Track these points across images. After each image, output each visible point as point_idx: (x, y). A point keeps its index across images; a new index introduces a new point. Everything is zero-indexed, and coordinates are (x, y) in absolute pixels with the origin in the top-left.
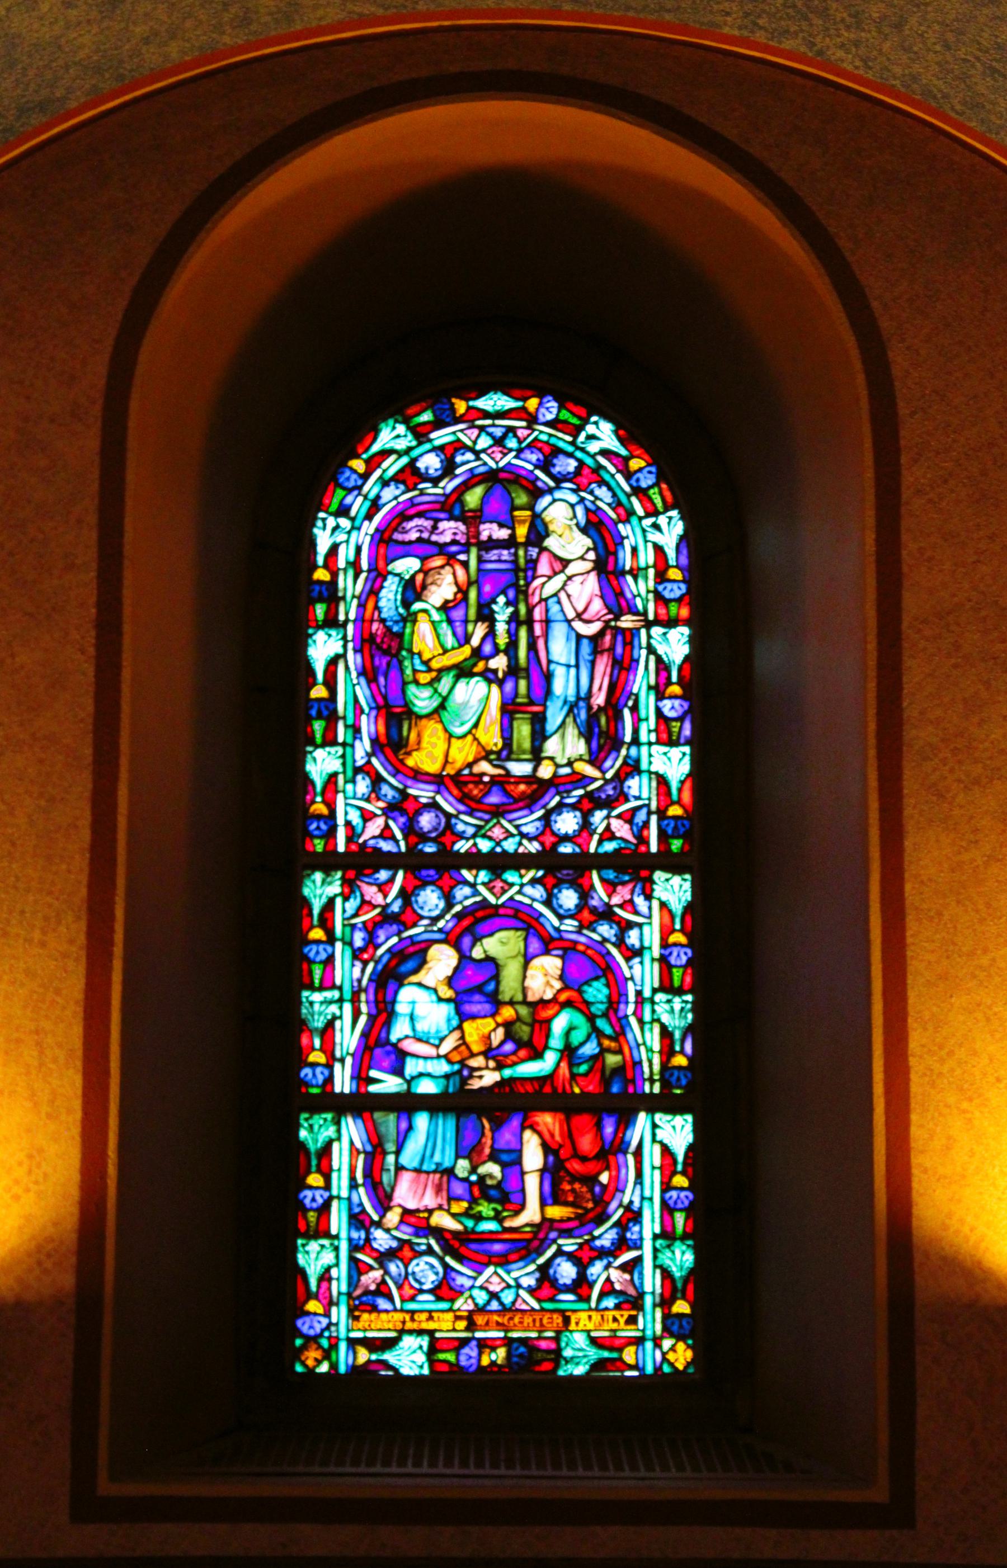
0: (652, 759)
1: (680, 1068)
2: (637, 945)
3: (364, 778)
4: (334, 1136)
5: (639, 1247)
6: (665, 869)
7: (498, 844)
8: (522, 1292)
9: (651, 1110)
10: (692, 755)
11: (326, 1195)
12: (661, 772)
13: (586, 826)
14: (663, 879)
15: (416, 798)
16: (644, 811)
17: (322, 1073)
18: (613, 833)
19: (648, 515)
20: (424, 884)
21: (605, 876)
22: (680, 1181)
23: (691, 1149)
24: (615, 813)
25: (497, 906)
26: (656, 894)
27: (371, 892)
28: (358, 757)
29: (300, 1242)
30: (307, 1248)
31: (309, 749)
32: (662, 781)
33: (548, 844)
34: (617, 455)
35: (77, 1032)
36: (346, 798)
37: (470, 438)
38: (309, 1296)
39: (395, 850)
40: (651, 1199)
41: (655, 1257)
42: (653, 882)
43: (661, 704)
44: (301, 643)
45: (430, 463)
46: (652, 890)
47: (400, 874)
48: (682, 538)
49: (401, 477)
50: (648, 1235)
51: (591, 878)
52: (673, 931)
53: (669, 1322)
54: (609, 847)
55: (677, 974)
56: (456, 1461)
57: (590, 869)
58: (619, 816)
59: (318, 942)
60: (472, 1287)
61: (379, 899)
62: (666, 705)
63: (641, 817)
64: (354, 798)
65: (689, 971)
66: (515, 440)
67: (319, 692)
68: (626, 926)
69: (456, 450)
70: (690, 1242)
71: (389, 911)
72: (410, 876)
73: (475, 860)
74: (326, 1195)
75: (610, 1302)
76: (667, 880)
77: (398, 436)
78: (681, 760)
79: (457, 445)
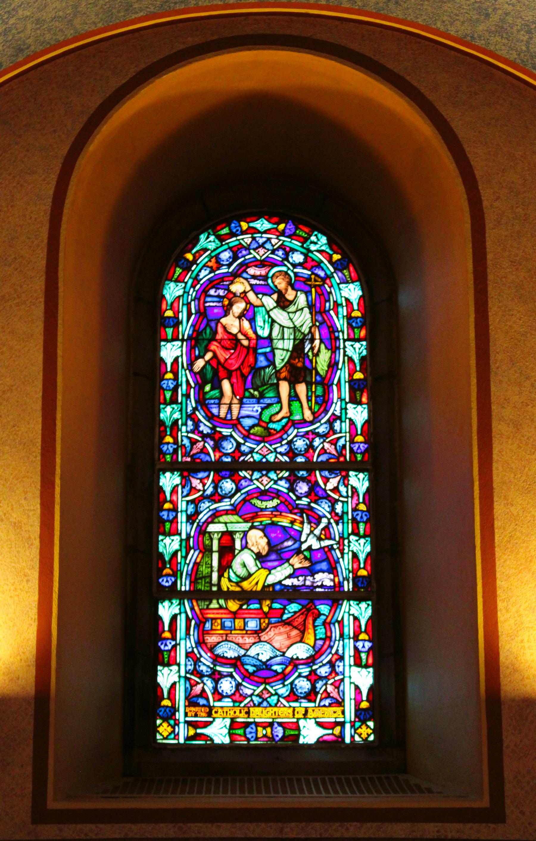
0: (351, 607)
3: (193, 508)
7: (264, 457)
8: (281, 699)
9: (349, 600)
10: (372, 605)
11: (173, 643)
15: (220, 432)
16: (343, 439)
17: (172, 383)
18: (326, 450)
20: (224, 478)
21: (323, 474)
22: (360, 438)
25: (265, 442)
28: (189, 411)
30: (165, 409)
36: (182, 433)
38: (165, 501)
40: (346, 569)
42: (349, 476)
44: (157, 349)
45: (226, 256)
47: (212, 473)
48: (369, 554)
49: (309, 260)
51: (315, 476)
52: (356, 371)
53: (358, 713)
54: (323, 458)
56: (246, 789)
57: (315, 470)
60: (252, 695)
62: (360, 645)
63: (341, 442)
65: (371, 653)
66: (270, 245)
67: (166, 703)
68: (334, 502)
69: (239, 249)
73: (277, 466)
74: (173, 643)
75: (327, 702)
76: (355, 408)
78: (366, 608)
79: (239, 247)
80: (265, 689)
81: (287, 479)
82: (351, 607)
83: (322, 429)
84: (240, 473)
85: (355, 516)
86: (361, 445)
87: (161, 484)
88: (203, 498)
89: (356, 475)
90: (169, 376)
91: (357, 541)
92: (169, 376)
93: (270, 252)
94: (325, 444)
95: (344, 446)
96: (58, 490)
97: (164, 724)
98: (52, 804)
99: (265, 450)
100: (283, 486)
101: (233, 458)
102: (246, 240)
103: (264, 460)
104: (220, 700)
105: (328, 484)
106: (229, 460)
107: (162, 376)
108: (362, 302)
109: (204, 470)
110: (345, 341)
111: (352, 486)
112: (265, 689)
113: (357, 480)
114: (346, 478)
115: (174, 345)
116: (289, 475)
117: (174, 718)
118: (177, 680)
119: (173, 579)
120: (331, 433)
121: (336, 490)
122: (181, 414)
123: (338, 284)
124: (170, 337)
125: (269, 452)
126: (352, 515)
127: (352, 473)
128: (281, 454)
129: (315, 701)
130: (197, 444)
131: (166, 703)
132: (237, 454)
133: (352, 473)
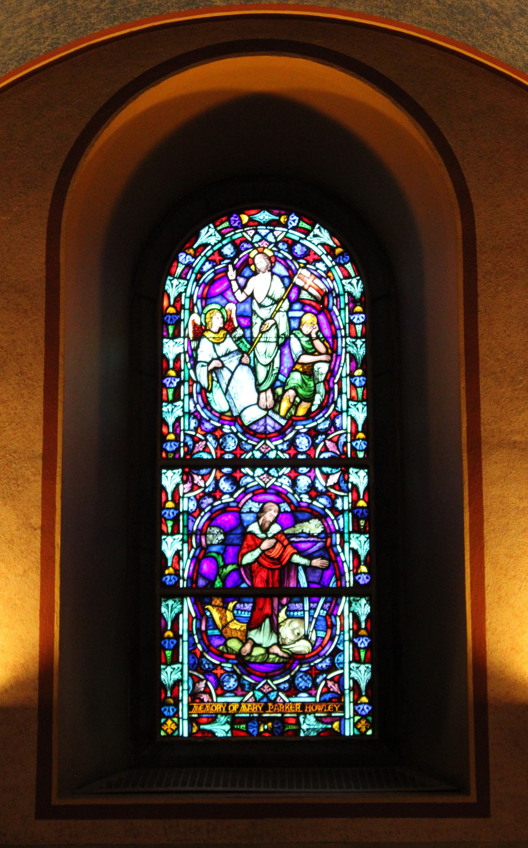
1: (362, 508)
2: (340, 508)
4: (180, 548)
5: (343, 668)
6: (355, 467)
12: (356, 679)
13: (314, 446)
14: (354, 472)
19: (345, 278)
23: (369, 553)
24: (329, 677)
26: (350, 480)
27: (197, 479)
29: (163, 667)
31: (163, 537)
32: (354, 421)
33: (292, 454)
34: (328, 245)
35: (35, 578)
37: (249, 236)
39: (209, 457)
41: (350, 674)
43: (357, 708)
46: (349, 478)
47: (317, 457)
50: (347, 661)
54: (326, 455)
55: (363, 654)
58: (332, 679)
59: (169, 638)
61: (328, 443)
63: (342, 440)
64: (189, 430)
70: (365, 403)
71: (206, 611)
72: (218, 472)
73: (278, 464)
77: (211, 235)
79: (242, 239)
80: (267, 683)
81: (288, 475)
82: (351, 672)
83: (324, 425)
84: (243, 470)
85: (353, 381)
86: (365, 707)
87: (164, 352)
88: (205, 495)
89: (357, 473)
90: (170, 504)
91: (358, 668)
92: (170, 504)
93: (272, 245)
94: (327, 442)
95: (345, 444)
96: (59, 470)
97: (165, 728)
98: (55, 801)
99: (266, 687)
100: (285, 483)
101: (235, 455)
102: (249, 232)
103: (266, 469)
104: (222, 695)
105: (329, 480)
106: (231, 456)
107: (164, 372)
108: (368, 558)
109: (206, 467)
110: (350, 533)
111: (352, 483)
112: (267, 683)
113: (357, 477)
114: (345, 473)
115: (174, 539)
116: (290, 472)
117: (177, 715)
118: (181, 414)
119: (175, 642)
120: (333, 429)
121: (336, 486)
122: (182, 674)
123: (341, 280)
124: (171, 397)
125: (270, 689)
126: (349, 318)
127: (351, 470)
128: (283, 451)
129: (315, 696)
130: (200, 443)
131: (170, 634)
132: (238, 451)
133: (351, 470)
